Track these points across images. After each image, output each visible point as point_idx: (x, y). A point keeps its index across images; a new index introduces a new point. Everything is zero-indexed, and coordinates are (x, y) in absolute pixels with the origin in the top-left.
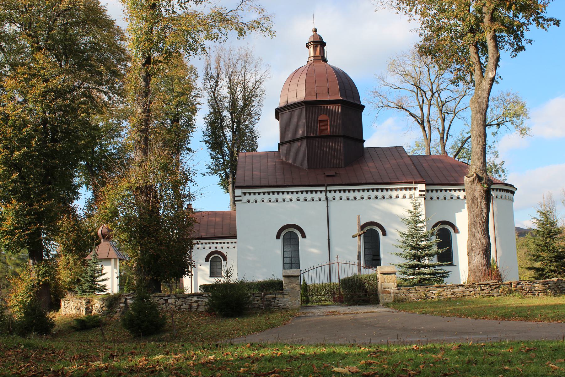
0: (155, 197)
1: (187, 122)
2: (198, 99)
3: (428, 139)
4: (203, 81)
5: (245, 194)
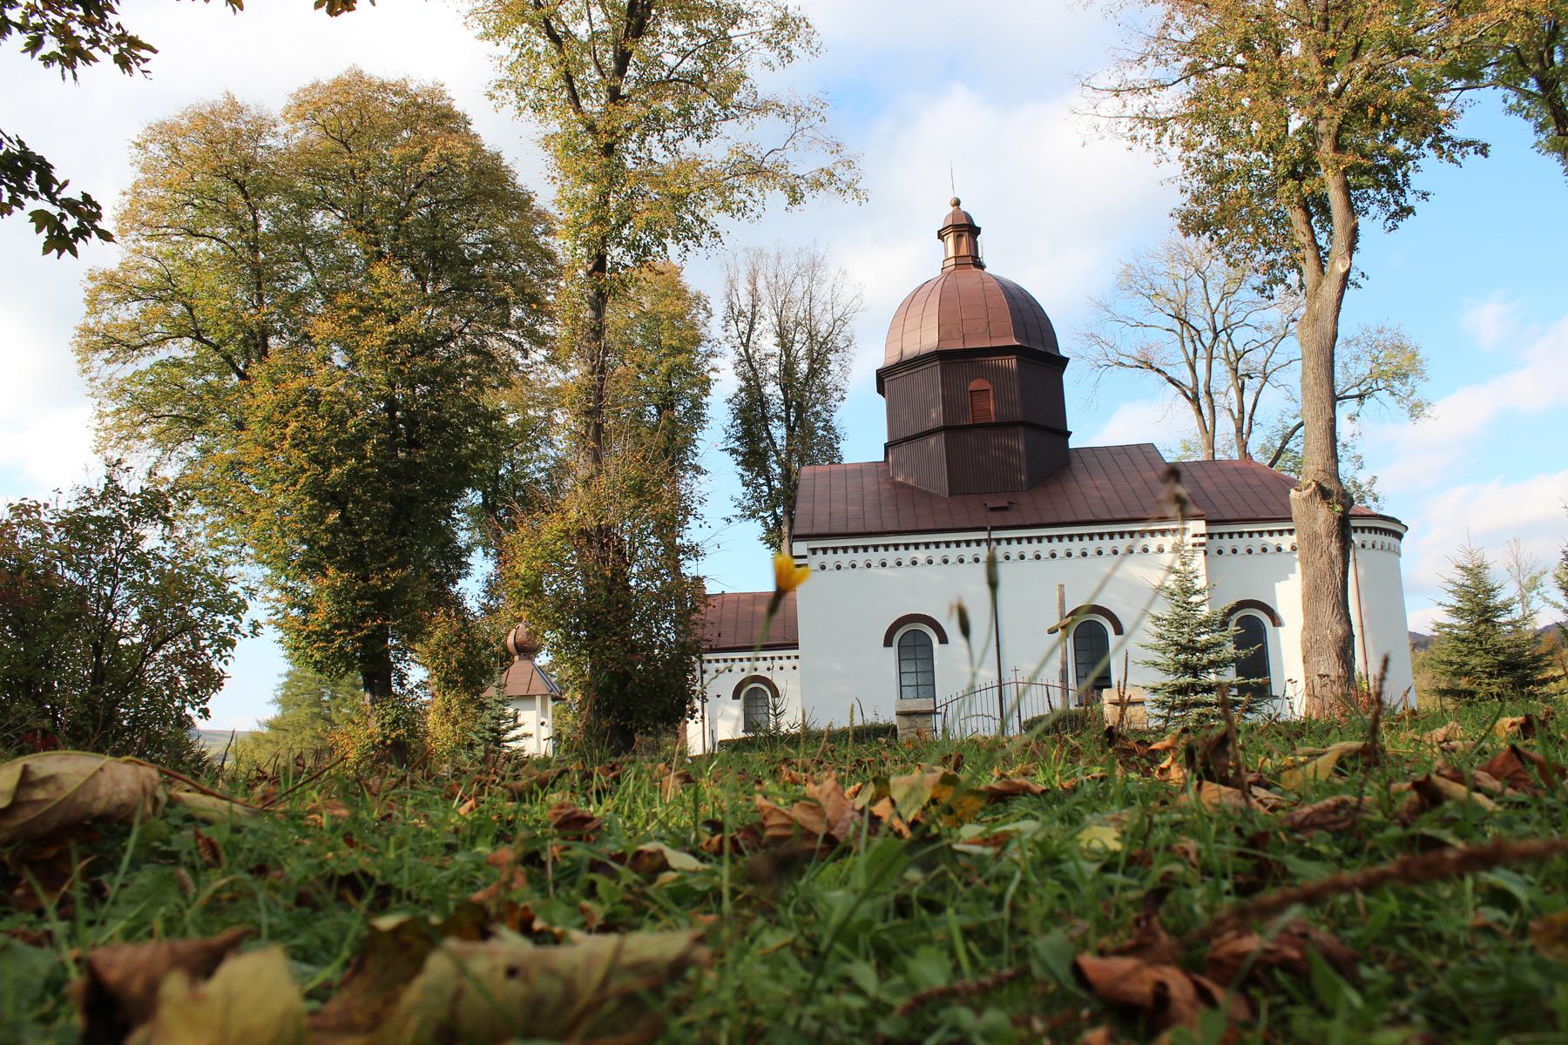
0: (620, 552)
1: (690, 409)
2: (713, 361)
3: (1209, 434)
4: (724, 323)
5: (814, 551)
